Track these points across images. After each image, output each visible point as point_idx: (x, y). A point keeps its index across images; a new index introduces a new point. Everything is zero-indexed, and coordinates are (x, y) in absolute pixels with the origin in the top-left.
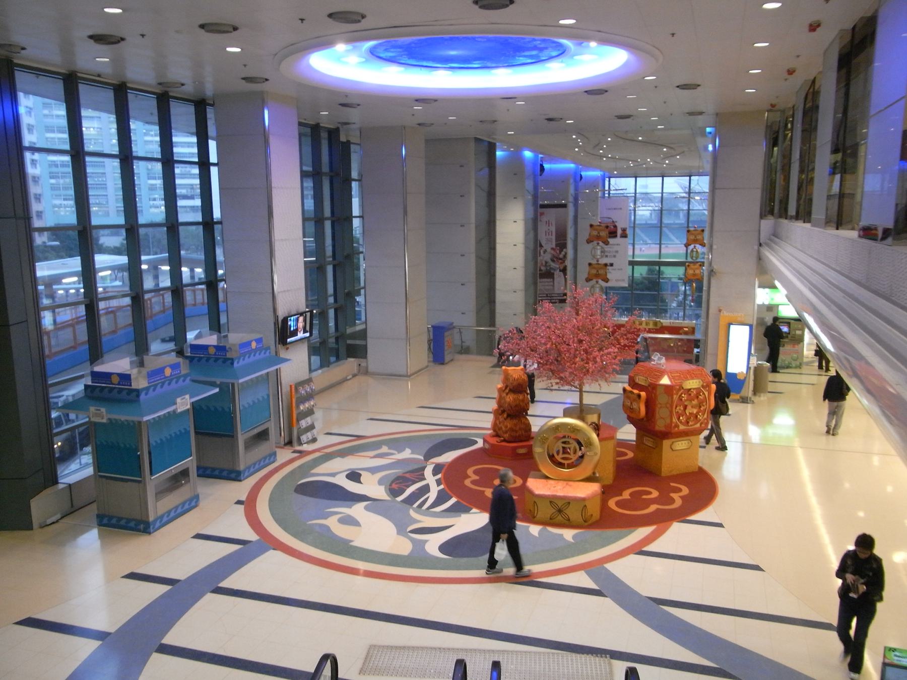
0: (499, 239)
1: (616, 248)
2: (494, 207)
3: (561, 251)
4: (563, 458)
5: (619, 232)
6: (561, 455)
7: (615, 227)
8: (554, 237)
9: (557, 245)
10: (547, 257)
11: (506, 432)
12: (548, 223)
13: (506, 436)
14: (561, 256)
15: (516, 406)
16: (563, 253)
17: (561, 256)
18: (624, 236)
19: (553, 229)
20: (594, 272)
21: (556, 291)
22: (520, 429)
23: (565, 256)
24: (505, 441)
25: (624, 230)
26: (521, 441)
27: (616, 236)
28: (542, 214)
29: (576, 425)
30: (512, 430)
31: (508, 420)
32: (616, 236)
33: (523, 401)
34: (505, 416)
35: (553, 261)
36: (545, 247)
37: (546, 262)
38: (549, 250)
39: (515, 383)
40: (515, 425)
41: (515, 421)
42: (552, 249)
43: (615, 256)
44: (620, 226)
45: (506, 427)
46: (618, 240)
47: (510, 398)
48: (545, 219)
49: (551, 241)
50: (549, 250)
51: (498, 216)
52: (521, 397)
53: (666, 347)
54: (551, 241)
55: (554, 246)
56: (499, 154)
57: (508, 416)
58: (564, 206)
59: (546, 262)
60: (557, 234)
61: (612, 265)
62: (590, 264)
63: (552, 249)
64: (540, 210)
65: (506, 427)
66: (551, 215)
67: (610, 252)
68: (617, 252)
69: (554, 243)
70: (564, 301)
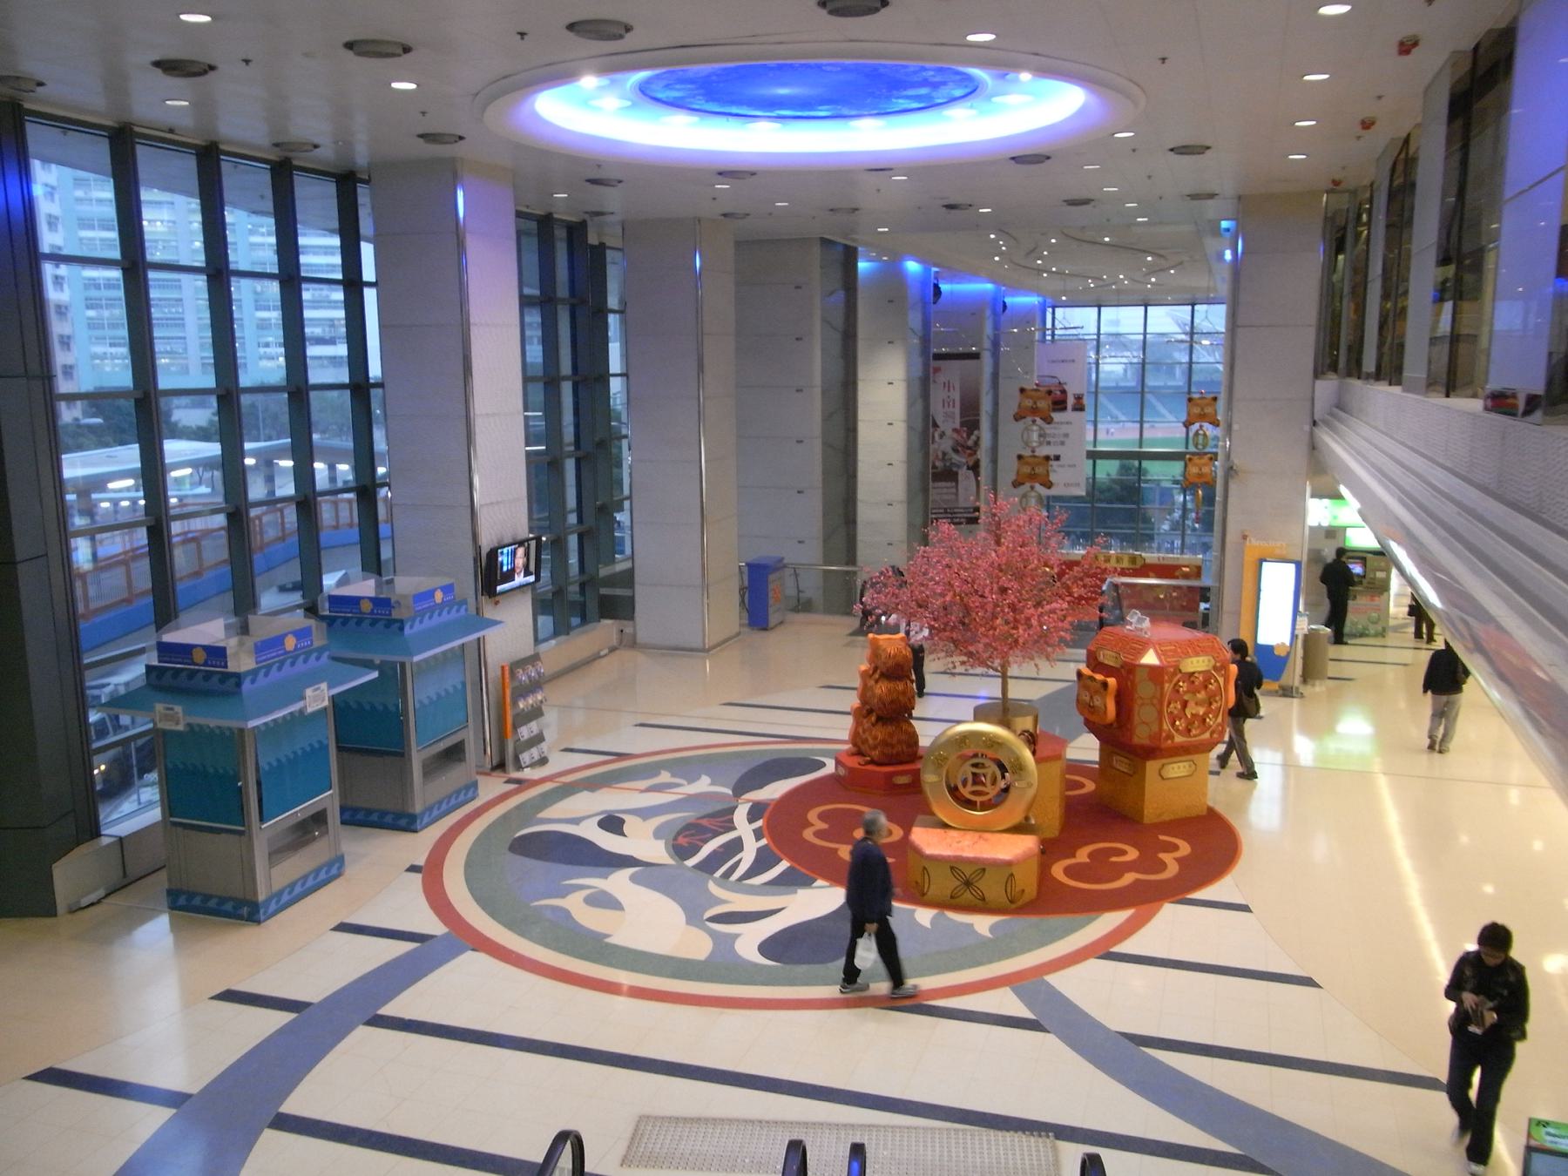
0: (863, 414)
1: (1064, 429)
2: (855, 358)
3: (970, 434)
4: (974, 793)
5: (1071, 401)
6: (970, 788)
7: (1064, 392)
8: (957, 411)
9: (962, 424)
10: (946, 445)
11: (875, 748)
12: (948, 386)
13: (876, 754)
14: (970, 443)
15: (892, 702)
16: (973, 438)
17: (970, 443)
18: (1079, 407)
19: (956, 396)
20: (1027, 470)
21: (962, 503)
22: (899, 742)
23: (977, 443)
24: (872, 762)
25: (1079, 398)
26: (901, 763)
27: (1065, 409)
28: (937, 370)
29: (996, 736)
30: (885, 743)
31: (879, 727)
32: (1065, 409)
33: (904, 693)
34: (873, 719)
35: (956, 451)
36: (942, 428)
37: (944, 454)
38: (949, 432)
39: (891, 663)
40: (891, 735)
41: (890, 729)
42: (955, 430)
43: (1063, 443)
44: (1072, 391)
45: (875, 738)
46: (1069, 415)
47: (882, 688)
48: (941, 378)
49: (952, 416)
50: (949, 432)
51: (861, 374)
52: (901, 686)
53: (1151, 600)
54: (952, 416)
55: (957, 425)
56: (863, 265)
57: (879, 719)
58: (976, 356)
59: (944, 454)
60: (962, 404)
61: (1057, 458)
62: (1020, 457)
63: (955, 430)
64: (934, 364)
65: (875, 738)
66: (953, 372)
67: (1054, 436)
68: (1066, 435)
69: (958, 421)
70: (975, 521)
